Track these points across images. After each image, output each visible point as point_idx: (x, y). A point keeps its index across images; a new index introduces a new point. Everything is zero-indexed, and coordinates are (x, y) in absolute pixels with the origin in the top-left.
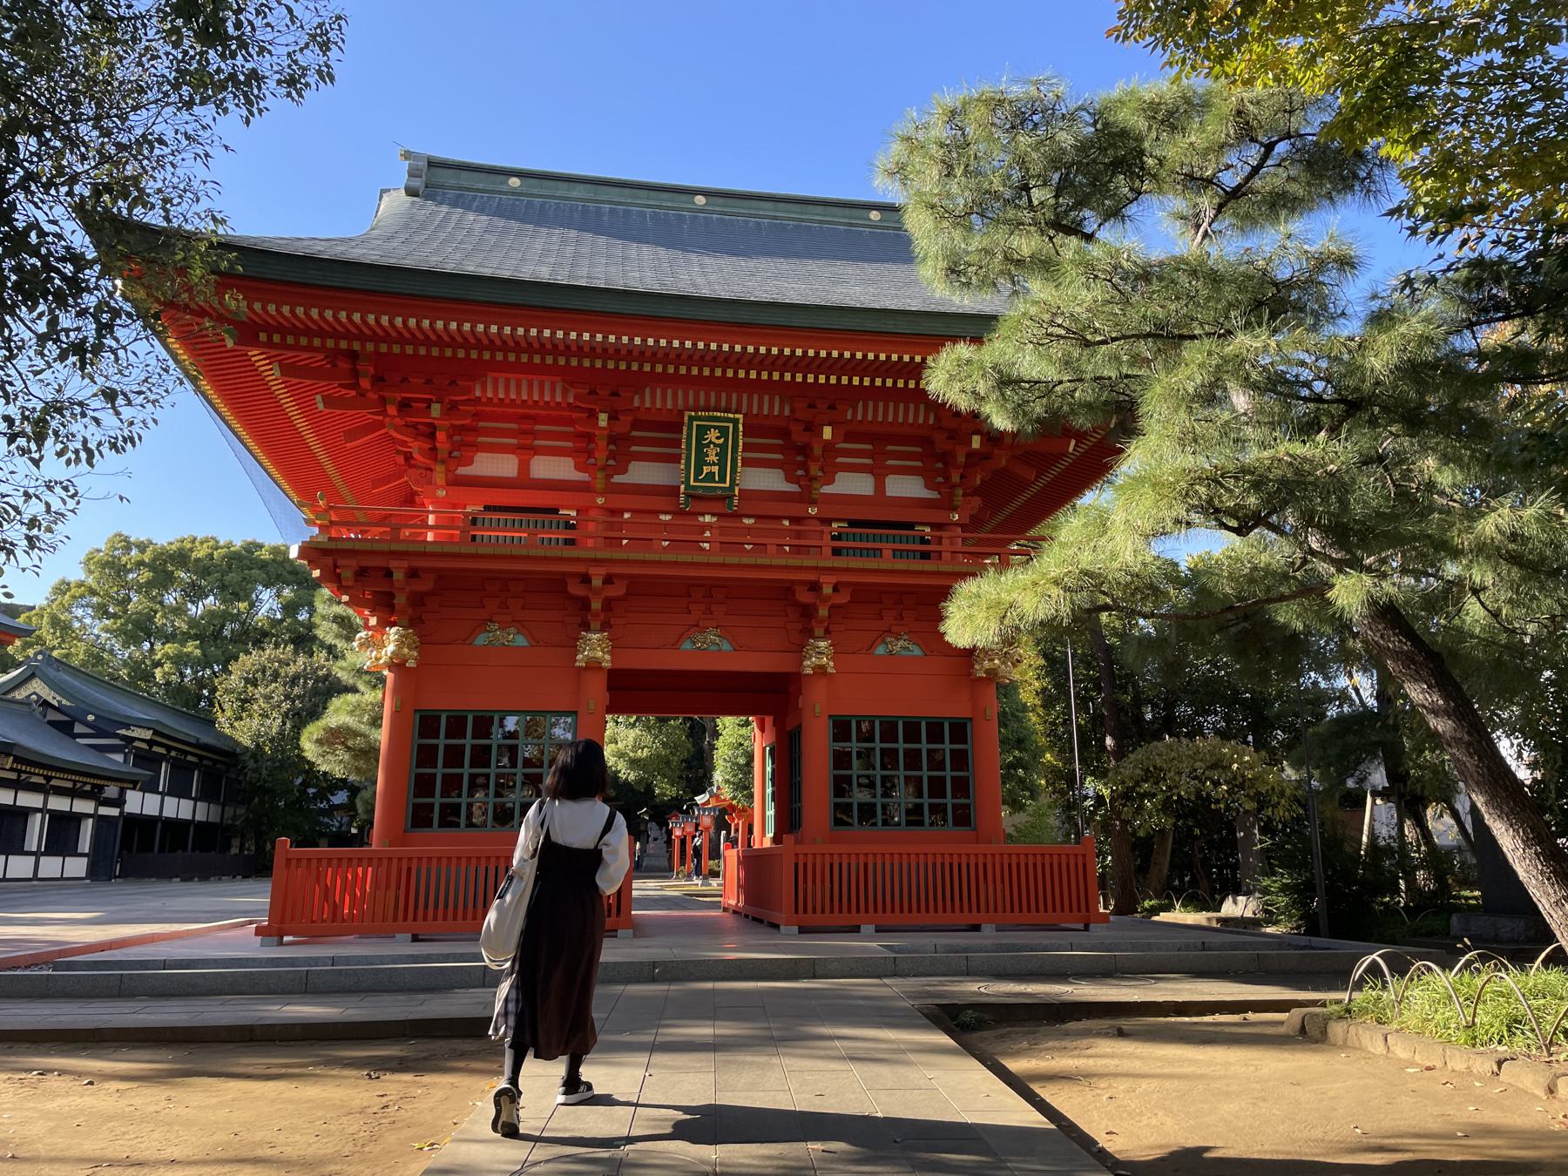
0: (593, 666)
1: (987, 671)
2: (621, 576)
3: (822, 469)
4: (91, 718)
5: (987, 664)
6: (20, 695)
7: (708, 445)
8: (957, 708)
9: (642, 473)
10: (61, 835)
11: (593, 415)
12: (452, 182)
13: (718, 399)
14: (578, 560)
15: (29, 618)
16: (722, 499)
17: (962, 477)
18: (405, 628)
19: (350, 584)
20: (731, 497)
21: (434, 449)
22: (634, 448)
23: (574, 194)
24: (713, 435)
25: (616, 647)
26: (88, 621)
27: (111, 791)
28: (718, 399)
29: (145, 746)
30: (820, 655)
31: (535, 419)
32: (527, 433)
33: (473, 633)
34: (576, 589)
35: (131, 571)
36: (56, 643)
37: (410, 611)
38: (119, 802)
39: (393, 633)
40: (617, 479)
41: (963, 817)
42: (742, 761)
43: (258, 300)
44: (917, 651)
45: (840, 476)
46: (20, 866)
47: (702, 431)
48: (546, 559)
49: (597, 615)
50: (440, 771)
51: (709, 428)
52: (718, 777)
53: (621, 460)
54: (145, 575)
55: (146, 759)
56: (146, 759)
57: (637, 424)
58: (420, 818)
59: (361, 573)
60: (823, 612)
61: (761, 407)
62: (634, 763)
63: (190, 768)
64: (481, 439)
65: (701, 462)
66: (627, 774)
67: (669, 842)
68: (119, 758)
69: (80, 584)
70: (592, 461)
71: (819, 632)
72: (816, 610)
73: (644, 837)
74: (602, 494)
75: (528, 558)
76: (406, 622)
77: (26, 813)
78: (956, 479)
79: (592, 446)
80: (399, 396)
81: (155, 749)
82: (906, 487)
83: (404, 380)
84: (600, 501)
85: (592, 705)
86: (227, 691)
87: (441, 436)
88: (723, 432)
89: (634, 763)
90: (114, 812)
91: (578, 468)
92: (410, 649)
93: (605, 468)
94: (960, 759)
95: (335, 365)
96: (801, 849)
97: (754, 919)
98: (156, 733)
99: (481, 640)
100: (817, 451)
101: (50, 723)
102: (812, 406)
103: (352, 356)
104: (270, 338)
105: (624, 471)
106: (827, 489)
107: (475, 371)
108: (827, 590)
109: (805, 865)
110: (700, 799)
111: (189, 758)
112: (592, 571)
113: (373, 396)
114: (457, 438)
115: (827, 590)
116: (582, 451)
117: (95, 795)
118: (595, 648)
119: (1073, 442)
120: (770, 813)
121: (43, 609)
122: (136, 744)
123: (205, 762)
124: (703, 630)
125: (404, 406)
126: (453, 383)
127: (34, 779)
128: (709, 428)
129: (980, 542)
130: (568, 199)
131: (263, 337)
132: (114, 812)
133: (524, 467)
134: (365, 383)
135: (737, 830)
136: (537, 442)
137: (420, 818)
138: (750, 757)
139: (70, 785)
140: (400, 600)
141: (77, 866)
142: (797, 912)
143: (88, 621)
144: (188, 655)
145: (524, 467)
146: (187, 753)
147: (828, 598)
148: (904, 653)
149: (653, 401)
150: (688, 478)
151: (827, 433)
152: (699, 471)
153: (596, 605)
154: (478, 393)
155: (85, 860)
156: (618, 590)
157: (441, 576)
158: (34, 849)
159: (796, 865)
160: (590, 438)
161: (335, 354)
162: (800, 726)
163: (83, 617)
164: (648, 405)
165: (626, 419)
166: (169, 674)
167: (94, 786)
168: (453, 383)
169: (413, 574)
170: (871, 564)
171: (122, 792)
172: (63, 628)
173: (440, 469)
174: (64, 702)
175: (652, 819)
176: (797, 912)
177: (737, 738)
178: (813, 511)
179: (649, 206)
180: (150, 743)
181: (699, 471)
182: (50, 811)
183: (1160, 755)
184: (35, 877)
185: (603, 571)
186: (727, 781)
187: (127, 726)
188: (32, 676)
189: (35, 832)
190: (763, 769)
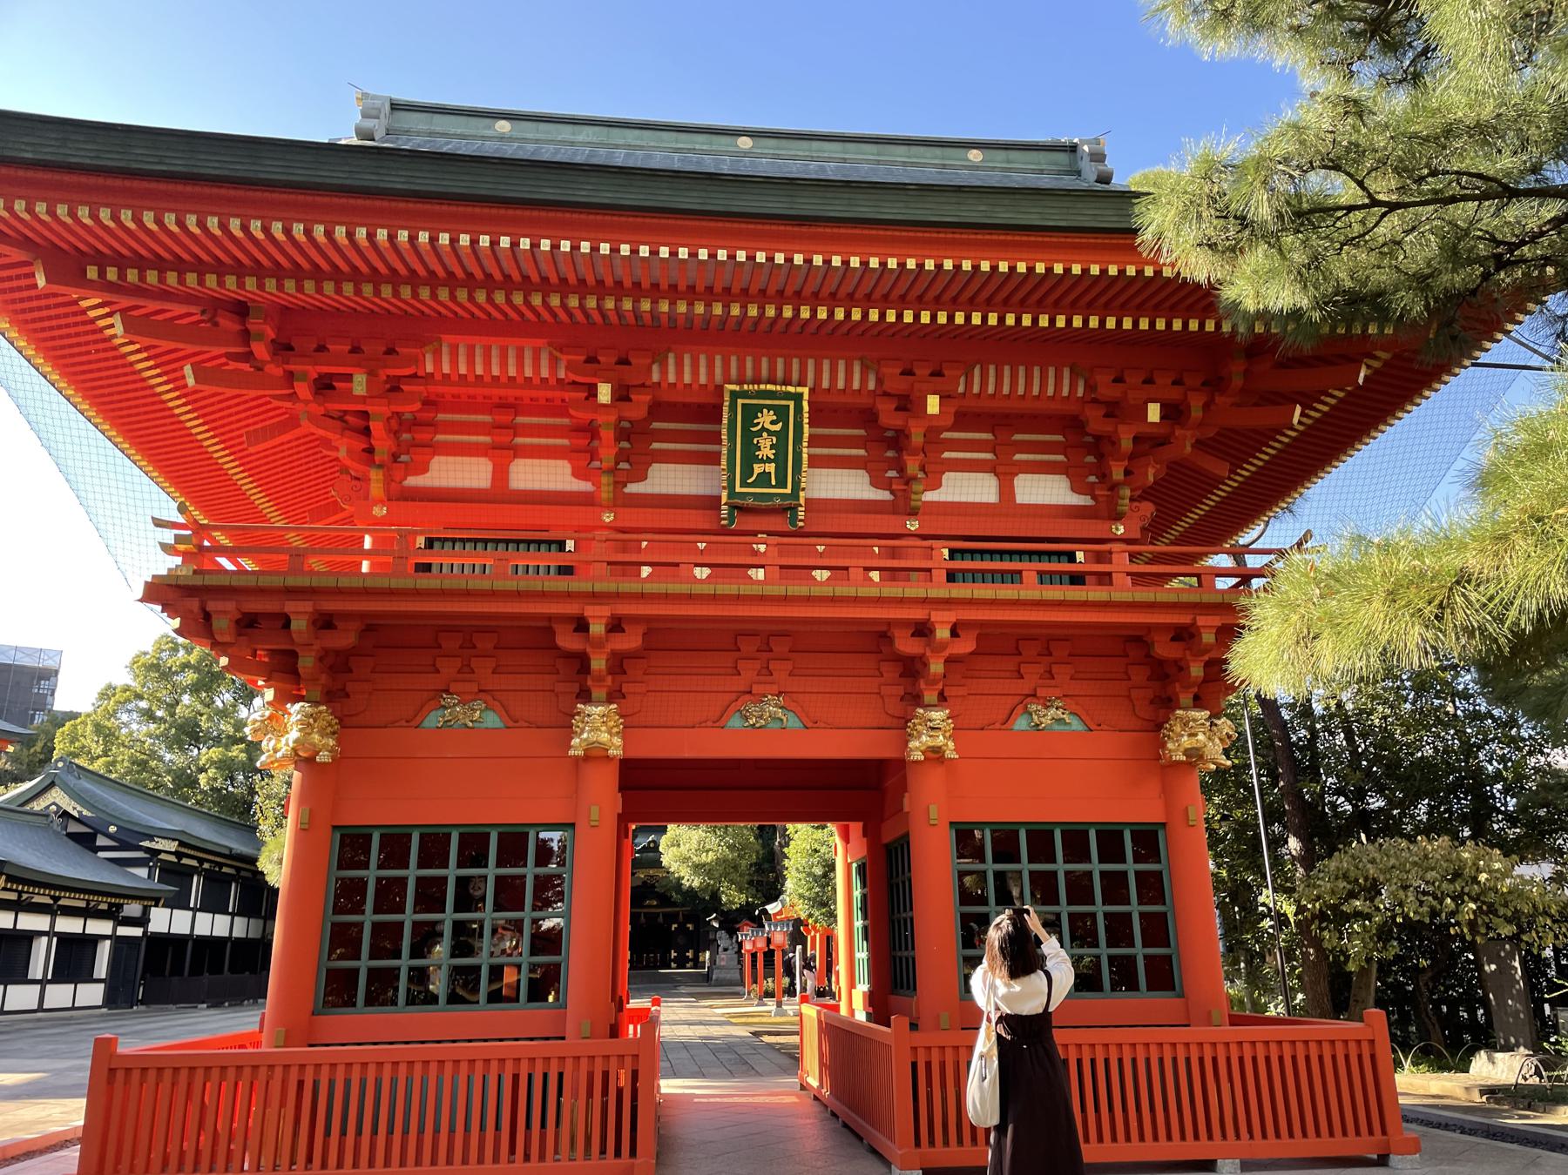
0: (596, 755)
1: (1187, 752)
2: (636, 620)
3: (923, 469)
4: (112, 829)
5: (1186, 742)
6: (38, 806)
7: (759, 434)
8: (1141, 808)
9: (668, 479)
10: (73, 959)
11: (592, 392)
12: (422, 127)
13: (772, 369)
14: (569, 596)
15: (75, 727)
16: (782, 510)
17: (1127, 473)
18: (316, 703)
19: (227, 639)
20: (794, 509)
21: (370, 451)
22: (656, 446)
23: (580, 138)
24: (766, 419)
25: (630, 725)
26: (134, 726)
27: (133, 909)
28: (772, 369)
29: (173, 859)
30: (933, 731)
31: (514, 407)
32: (505, 421)
33: (421, 710)
34: (567, 641)
35: (176, 673)
36: (99, 751)
37: (324, 678)
38: (143, 921)
39: (295, 709)
40: (632, 488)
41: (1163, 976)
42: (818, 871)
43: (62, 202)
44: (1076, 725)
45: (948, 478)
46: (20, 997)
47: (751, 413)
48: (519, 595)
49: (600, 679)
50: (368, 918)
51: (760, 408)
52: (789, 885)
53: (637, 460)
54: (190, 677)
55: (175, 874)
56: (175, 874)
57: (659, 409)
58: (339, 990)
59: (248, 623)
60: (937, 667)
61: (833, 378)
62: (697, 868)
63: (227, 880)
64: (440, 437)
65: (750, 458)
66: (691, 880)
67: (739, 952)
68: (143, 872)
69: (126, 689)
70: (596, 464)
71: (930, 697)
72: (926, 665)
73: (713, 947)
74: (611, 507)
75: (492, 594)
76: (317, 695)
77: (30, 937)
78: (1118, 474)
79: (596, 443)
80: (314, 371)
81: (185, 861)
82: (1044, 490)
83: (321, 348)
84: (608, 518)
85: (595, 813)
86: (268, 797)
87: (376, 426)
88: (782, 414)
89: (697, 868)
90: (137, 932)
91: (577, 474)
92: (323, 734)
93: (613, 471)
94: (1152, 887)
95: (216, 324)
96: (920, 1039)
97: (845, 1125)
98: (182, 844)
99: (433, 720)
100: (917, 438)
101: (70, 835)
102: (908, 372)
103: (241, 309)
104: (102, 274)
105: (643, 477)
106: (930, 496)
107: (424, 328)
108: (943, 633)
109: (928, 1065)
110: (772, 908)
111: (225, 870)
112: (589, 611)
113: (274, 370)
114: (406, 436)
115: (943, 633)
116: (582, 445)
117: (113, 914)
118: (598, 728)
119: (1298, 409)
120: (862, 955)
121: (88, 715)
122: (162, 856)
123: (243, 873)
124: (759, 699)
125: (324, 386)
126: (390, 351)
127: (37, 899)
128: (760, 408)
129: (1157, 559)
130: (572, 143)
131: (92, 273)
132: (137, 932)
133: (501, 474)
134: (260, 349)
135: (813, 948)
136: (519, 440)
137: (339, 990)
138: (831, 867)
139: (82, 904)
140: (306, 662)
141: (92, 994)
142: (918, 1145)
143: (134, 726)
144: (232, 759)
145: (501, 474)
146: (221, 865)
147: (943, 645)
148: (1057, 727)
149: (682, 372)
150: (731, 480)
151: (933, 404)
152: (747, 472)
153: (598, 663)
154: (429, 368)
155: (102, 986)
156: (630, 641)
157: (371, 626)
158: (39, 977)
159: (914, 1065)
160: (591, 431)
161: (214, 305)
162: (907, 834)
163: (133, 726)
164: (672, 378)
165: (642, 399)
166: (215, 779)
167: (111, 905)
168: (390, 351)
169: (325, 622)
170: (1007, 592)
171: (146, 911)
172: (107, 735)
173: (376, 476)
174: (85, 812)
175: (721, 928)
176: (918, 1145)
177: (811, 845)
178: (913, 526)
179: (677, 150)
180: (176, 853)
181: (747, 472)
182: (58, 934)
183: (1373, 861)
184: (40, 1009)
185: (606, 611)
186: (801, 896)
187: (151, 838)
188: (52, 785)
189: (40, 958)
190: (847, 892)
